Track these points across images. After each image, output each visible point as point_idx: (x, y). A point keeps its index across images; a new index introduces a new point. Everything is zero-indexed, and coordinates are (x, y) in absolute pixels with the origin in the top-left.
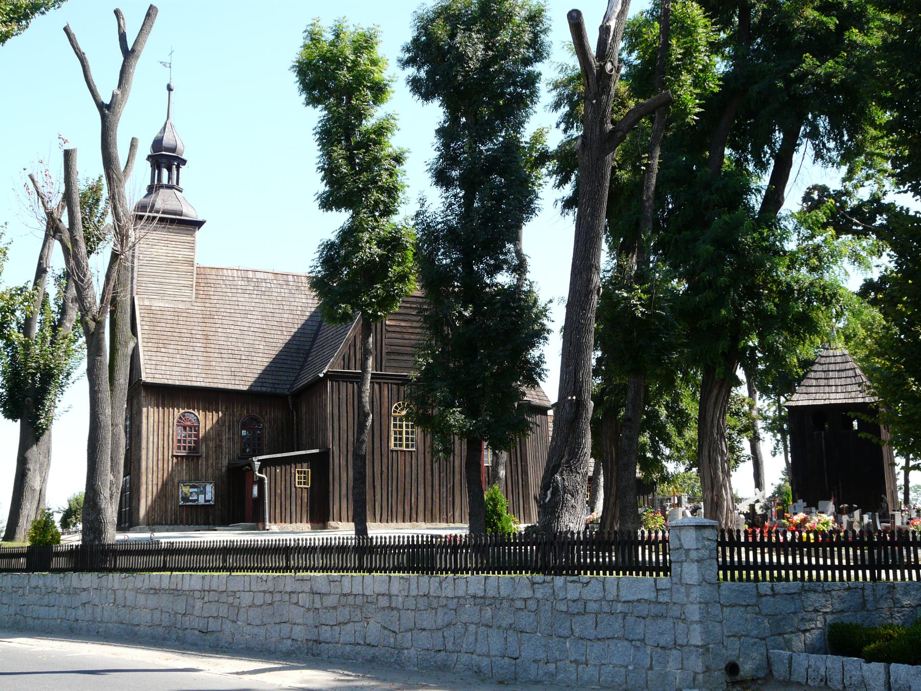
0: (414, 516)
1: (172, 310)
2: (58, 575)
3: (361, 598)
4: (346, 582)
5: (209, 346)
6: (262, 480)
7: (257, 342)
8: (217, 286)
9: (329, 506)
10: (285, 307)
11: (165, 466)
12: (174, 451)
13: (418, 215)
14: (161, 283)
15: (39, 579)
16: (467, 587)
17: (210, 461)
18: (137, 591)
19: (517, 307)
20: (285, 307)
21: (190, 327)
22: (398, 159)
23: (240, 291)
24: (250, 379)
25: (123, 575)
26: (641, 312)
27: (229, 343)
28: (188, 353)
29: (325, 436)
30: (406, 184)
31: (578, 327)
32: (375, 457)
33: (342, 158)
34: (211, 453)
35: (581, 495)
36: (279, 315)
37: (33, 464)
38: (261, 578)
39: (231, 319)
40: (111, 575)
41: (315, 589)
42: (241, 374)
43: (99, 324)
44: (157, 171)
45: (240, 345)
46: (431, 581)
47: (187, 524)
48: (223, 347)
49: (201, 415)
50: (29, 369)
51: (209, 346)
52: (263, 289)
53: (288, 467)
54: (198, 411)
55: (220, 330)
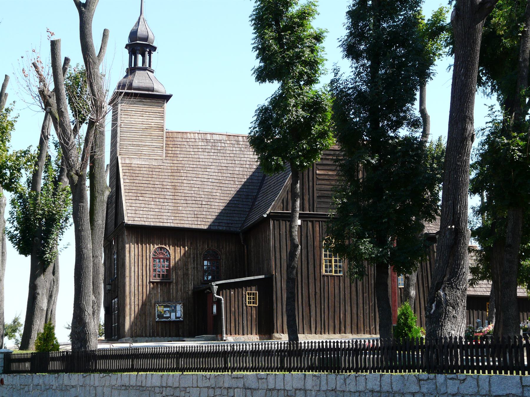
0: (343, 328)
1: (147, 166)
2: (54, 375)
3: (283, 392)
4: (271, 379)
5: (177, 194)
6: (219, 300)
7: (215, 191)
8: (183, 146)
9: (273, 321)
10: (237, 162)
11: (144, 290)
12: (151, 278)
13: (332, 82)
14: (138, 146)
15: (40, 378)
16: (366, 383)
17: (179, 286)
18: (112, 387)
19: (415, 155)
20: (237, 162)
21: (162, 180)
22: (318, 38)
23: (200, 150)
24: (209, 220)
25: (102, 375)
26: (518, 155)
27: (192, 192)
28: (160, 200)
29: (269, 264)
30: (325, 58)
31: (455, 168)
32: (310, 281)
33: (272, 39)
34: (179, 279)
35: (461, 307)
36: (232, 169)
37: (41, 290)
38: (206, 377)
39: (194, 172)
40: (92, 375)
41: (247, 385)
42: (202, 216)
43: (81, 178)
44: (133, 57)
45: (201, 193)
46: (338, 379)
47: (163, 336)
48: (188, 195)
49: (171, 250)
50: (37, 215)
51: (177, 194)
52: (219, 148)
53: (240, 290)
54: (169, 246)
55: (185, 181)
